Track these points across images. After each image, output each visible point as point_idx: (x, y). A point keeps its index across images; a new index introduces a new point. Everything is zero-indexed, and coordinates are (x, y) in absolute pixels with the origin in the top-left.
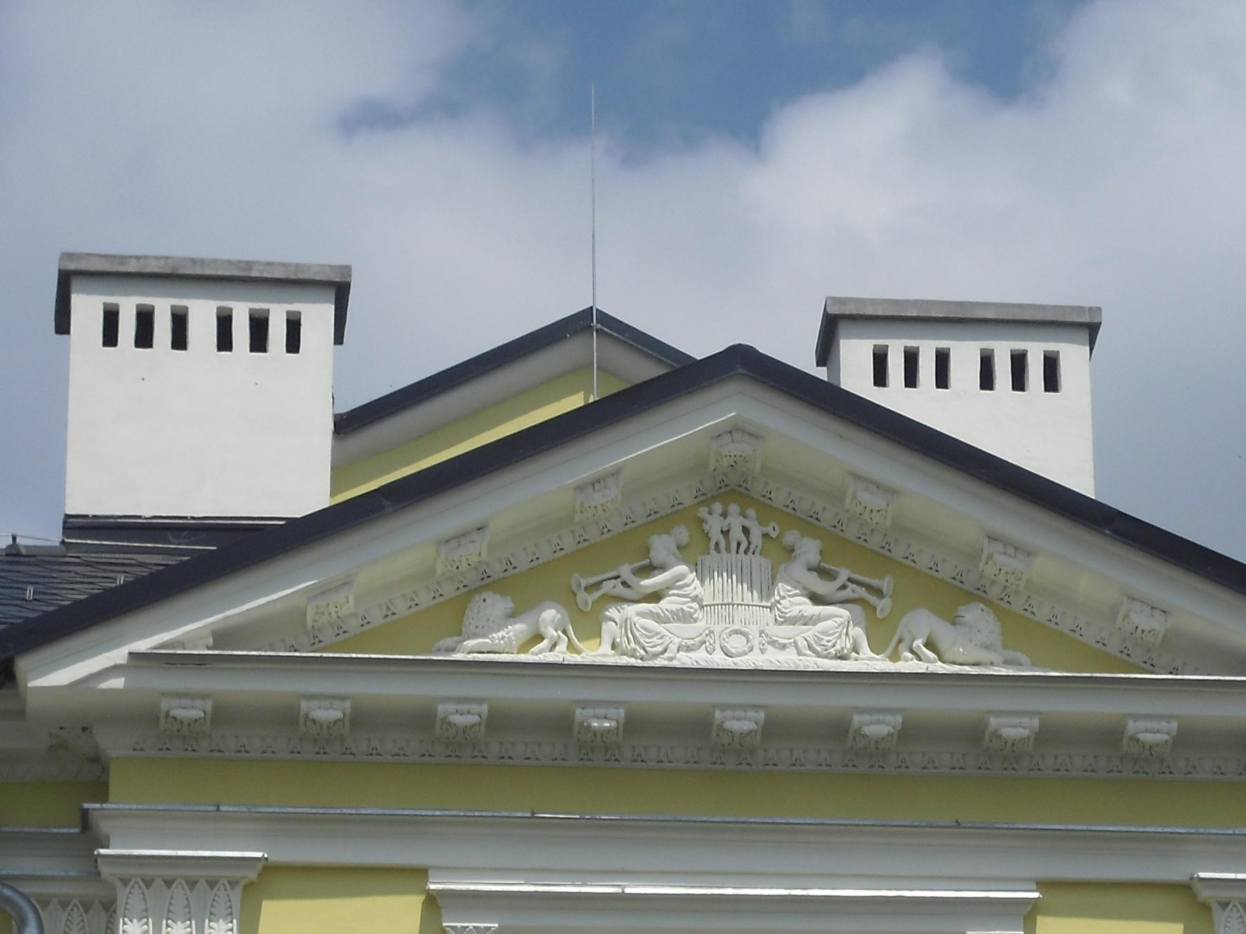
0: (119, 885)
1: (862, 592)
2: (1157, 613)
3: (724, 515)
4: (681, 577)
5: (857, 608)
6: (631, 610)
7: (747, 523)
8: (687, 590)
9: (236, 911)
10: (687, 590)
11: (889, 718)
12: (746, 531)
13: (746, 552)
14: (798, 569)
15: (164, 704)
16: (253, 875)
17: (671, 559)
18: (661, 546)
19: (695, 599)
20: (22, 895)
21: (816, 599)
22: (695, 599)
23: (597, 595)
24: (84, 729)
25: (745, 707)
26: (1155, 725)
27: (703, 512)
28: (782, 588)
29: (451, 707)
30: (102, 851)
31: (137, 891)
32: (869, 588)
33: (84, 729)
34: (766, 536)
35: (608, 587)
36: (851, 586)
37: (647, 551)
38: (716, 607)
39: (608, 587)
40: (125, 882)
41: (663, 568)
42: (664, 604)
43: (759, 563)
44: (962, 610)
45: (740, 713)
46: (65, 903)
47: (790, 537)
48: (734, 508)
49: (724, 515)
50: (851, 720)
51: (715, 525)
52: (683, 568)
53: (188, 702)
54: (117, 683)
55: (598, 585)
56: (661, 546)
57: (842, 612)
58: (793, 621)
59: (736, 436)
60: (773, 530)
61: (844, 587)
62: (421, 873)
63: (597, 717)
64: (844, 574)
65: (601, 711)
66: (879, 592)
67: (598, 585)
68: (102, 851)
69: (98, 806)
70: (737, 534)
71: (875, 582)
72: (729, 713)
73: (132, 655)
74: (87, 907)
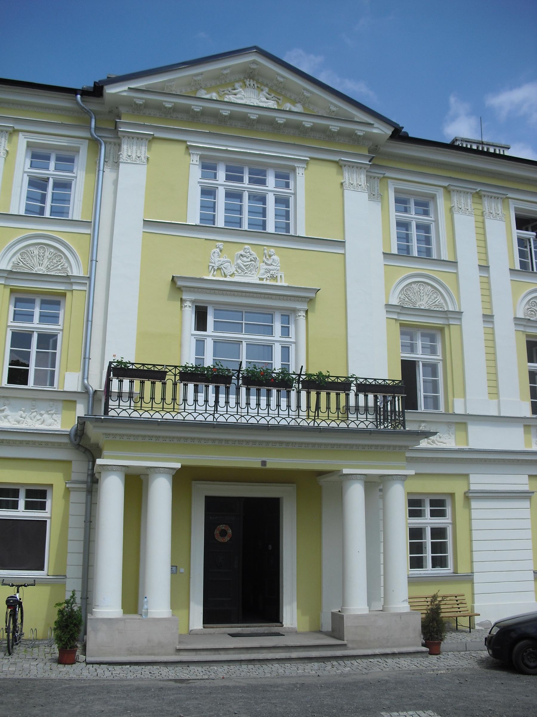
0: (122, 138)
1: (277, 99)
2: (335, 107)
3: (250, 81)
4: (241, 91)
5: (276, 102)
6: (231, 96)
7: (254, 83)
8: (242, 94)
9: (147, 145)
10: (242, 94)
11: (283, 120)
12: (254, 85)
13: (254, 88)
14: (264, 93)
15: (135, 100)
16: (151, 138)
17: (239, 88)
18: (237, 85)
19: (244, 96)
20: (103, 141)
21: (267, 99)
22: (244, 96)
23: (224, 93)
24: (117, 108)
25: (255, 114)
26: (335, 127)
27: (245, 80)
28: (261, 96)
29: (194, 107)
30: (120, 129)
31: (126, 139)
32: (278, 99)
33: (117, 108)
34: (258, 87)
35: (226, 92)
36: (274, 98)
37: (234, 86)
38: (248, 97)
39: (226, 92)
40: (124, 137)
41: (237, 89)
42: (237, 96)
43: (256, 91)
44: (296, 104)
45: (253, 115)
46: (110, 143)
47: (263, 87)
48: (251, 80)
49: (250, 81)
50: (275, 119)
51: (247, 83)
52: (241, 89)
53: (140, 100)
54: (125, 94)
55: (224, 91)
56: (237, 85)
57: (273, 102)
58: (263, 102)
59: (254, 64)
60: (259, 86)
61: (273, 98)
62: (185, 142)
63: (224, 112)
64: (273, 95)
65: (225, 111)
66: (280, 100)
67: (224, 91)
68: (120, 129)
69: (119, 120)
70: (252, 85)
71: (279, 97)
72: (251, 115)
73: (129, 88)
74: (115, 145)
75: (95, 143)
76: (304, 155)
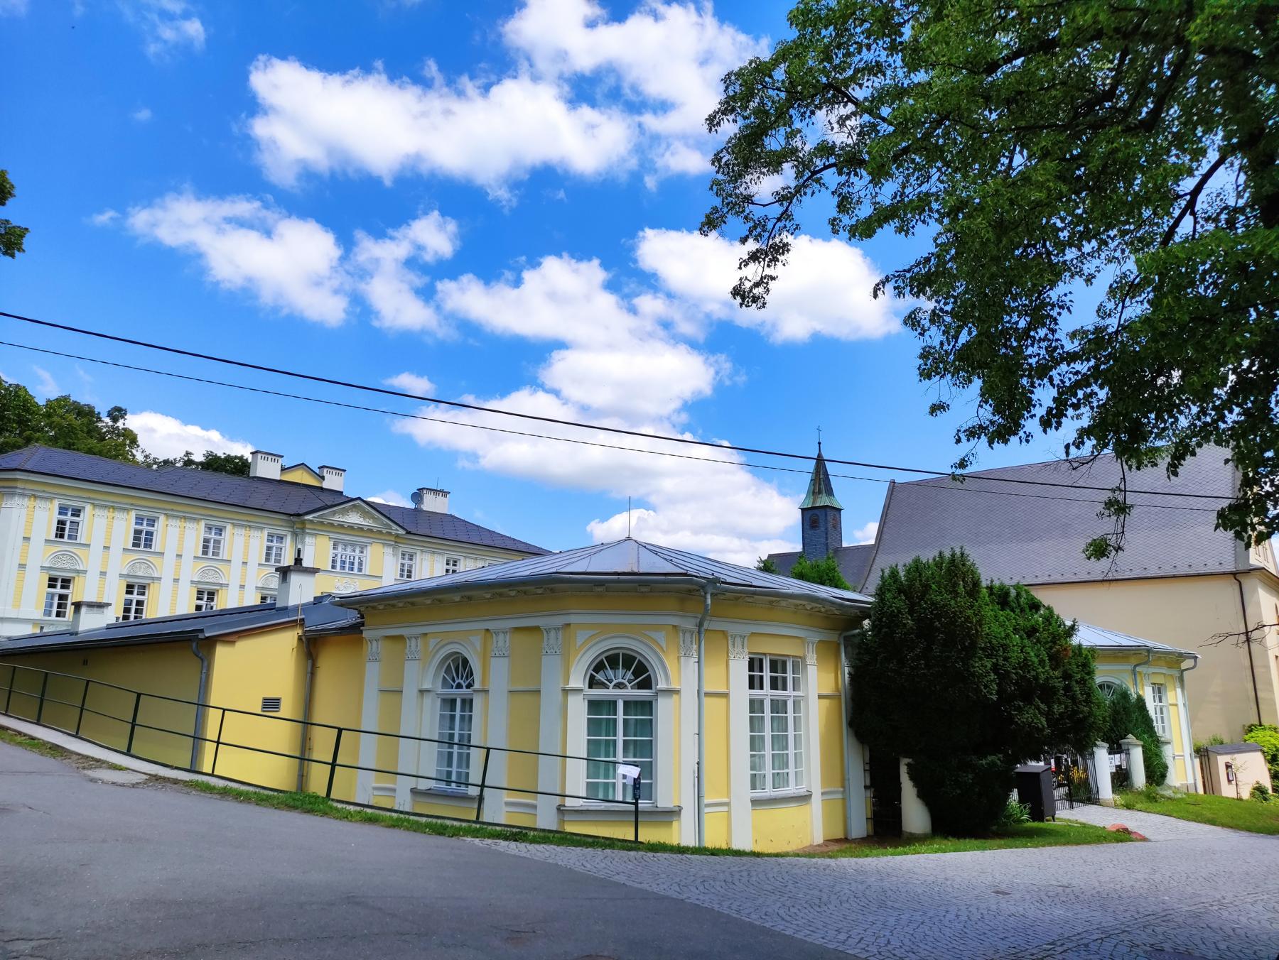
75: (295, 535)
76: (371, 540)
